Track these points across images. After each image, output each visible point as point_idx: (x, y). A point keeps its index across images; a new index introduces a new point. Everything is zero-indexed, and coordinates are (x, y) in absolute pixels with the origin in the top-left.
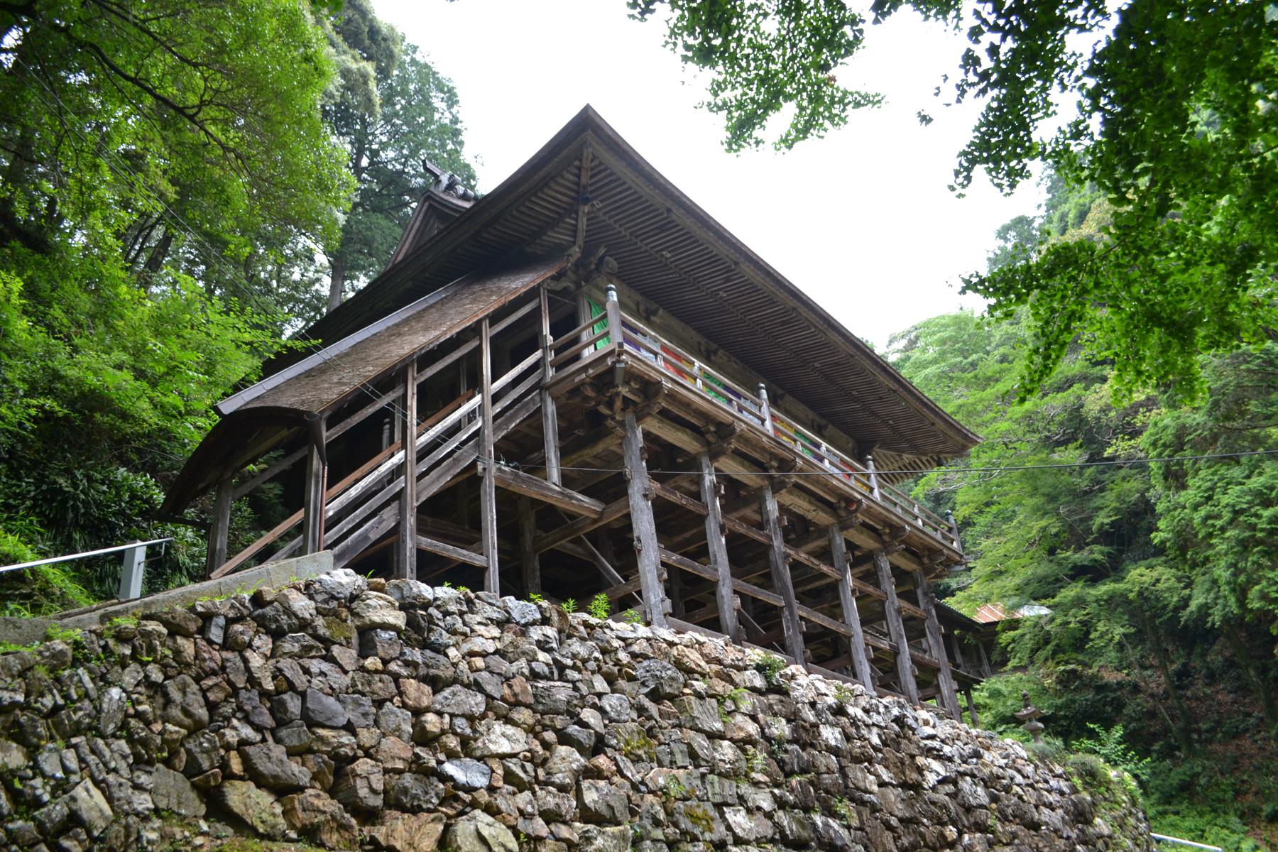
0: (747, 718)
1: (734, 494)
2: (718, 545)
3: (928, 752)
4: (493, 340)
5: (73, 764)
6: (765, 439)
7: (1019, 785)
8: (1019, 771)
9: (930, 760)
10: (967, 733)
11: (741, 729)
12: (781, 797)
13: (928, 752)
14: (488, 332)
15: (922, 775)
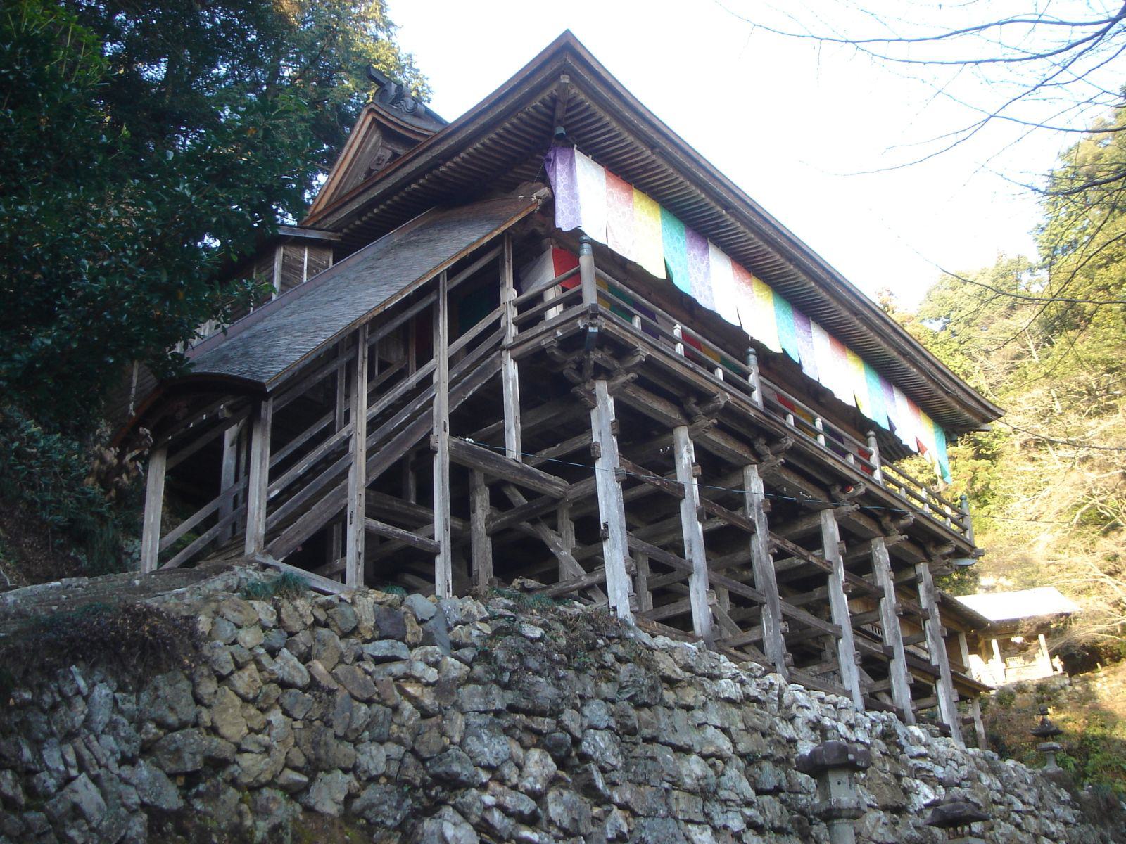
0: (718, 731)
1: (713, 468)
2: (686, 457)
3: (917, 772)
4: (451, 295)
5: (71, 758)
6: (752, 413)
7: (1017, 812)
8: (1019, 796)
9: (918, 782)
10: (963, 752)
11: (711, 743)
12: (750, 817)
13: (917, 772)
14: (445, 287)
15: (909, 798)
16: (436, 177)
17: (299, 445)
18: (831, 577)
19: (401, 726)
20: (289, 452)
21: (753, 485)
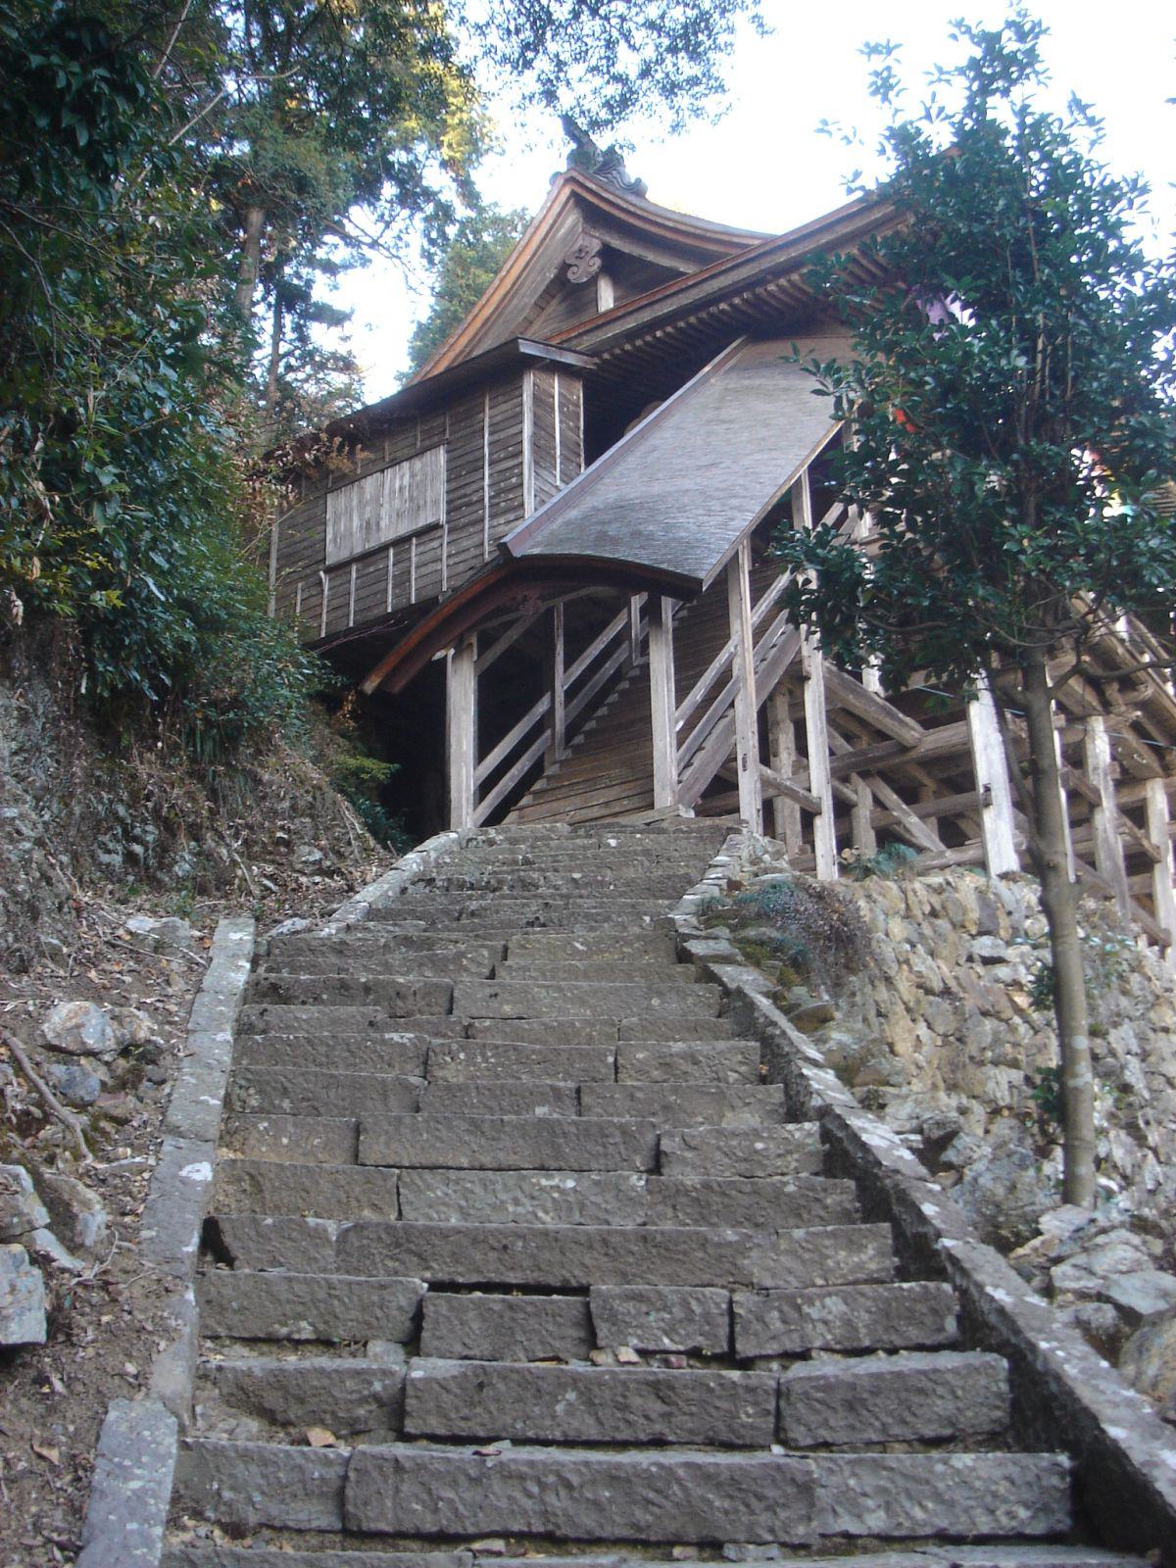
6: (1120, 650)
16: (757, 297)
17: (596, 652)
18: (1157, 867)
19: (1016, 1045)
20: (588, 662)
21: (1098, 742)
